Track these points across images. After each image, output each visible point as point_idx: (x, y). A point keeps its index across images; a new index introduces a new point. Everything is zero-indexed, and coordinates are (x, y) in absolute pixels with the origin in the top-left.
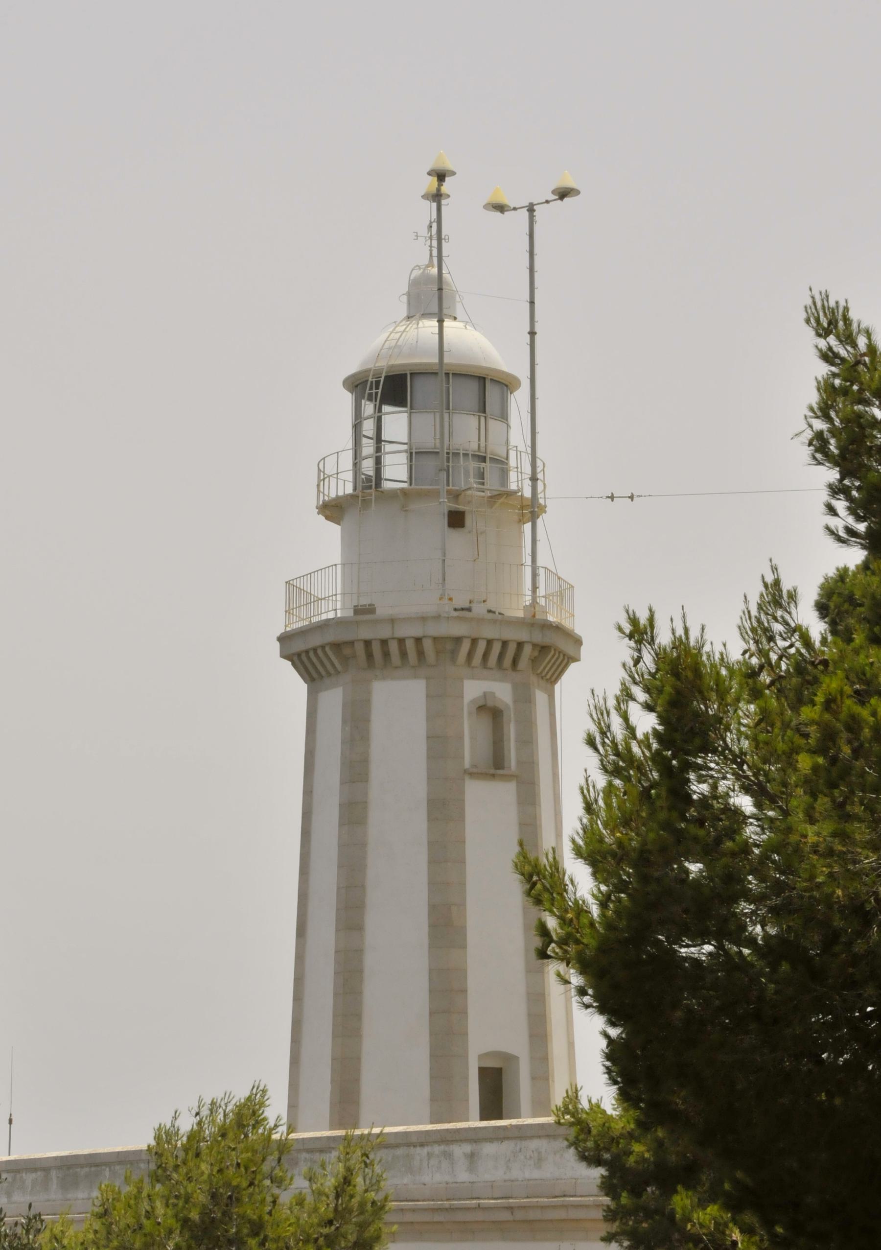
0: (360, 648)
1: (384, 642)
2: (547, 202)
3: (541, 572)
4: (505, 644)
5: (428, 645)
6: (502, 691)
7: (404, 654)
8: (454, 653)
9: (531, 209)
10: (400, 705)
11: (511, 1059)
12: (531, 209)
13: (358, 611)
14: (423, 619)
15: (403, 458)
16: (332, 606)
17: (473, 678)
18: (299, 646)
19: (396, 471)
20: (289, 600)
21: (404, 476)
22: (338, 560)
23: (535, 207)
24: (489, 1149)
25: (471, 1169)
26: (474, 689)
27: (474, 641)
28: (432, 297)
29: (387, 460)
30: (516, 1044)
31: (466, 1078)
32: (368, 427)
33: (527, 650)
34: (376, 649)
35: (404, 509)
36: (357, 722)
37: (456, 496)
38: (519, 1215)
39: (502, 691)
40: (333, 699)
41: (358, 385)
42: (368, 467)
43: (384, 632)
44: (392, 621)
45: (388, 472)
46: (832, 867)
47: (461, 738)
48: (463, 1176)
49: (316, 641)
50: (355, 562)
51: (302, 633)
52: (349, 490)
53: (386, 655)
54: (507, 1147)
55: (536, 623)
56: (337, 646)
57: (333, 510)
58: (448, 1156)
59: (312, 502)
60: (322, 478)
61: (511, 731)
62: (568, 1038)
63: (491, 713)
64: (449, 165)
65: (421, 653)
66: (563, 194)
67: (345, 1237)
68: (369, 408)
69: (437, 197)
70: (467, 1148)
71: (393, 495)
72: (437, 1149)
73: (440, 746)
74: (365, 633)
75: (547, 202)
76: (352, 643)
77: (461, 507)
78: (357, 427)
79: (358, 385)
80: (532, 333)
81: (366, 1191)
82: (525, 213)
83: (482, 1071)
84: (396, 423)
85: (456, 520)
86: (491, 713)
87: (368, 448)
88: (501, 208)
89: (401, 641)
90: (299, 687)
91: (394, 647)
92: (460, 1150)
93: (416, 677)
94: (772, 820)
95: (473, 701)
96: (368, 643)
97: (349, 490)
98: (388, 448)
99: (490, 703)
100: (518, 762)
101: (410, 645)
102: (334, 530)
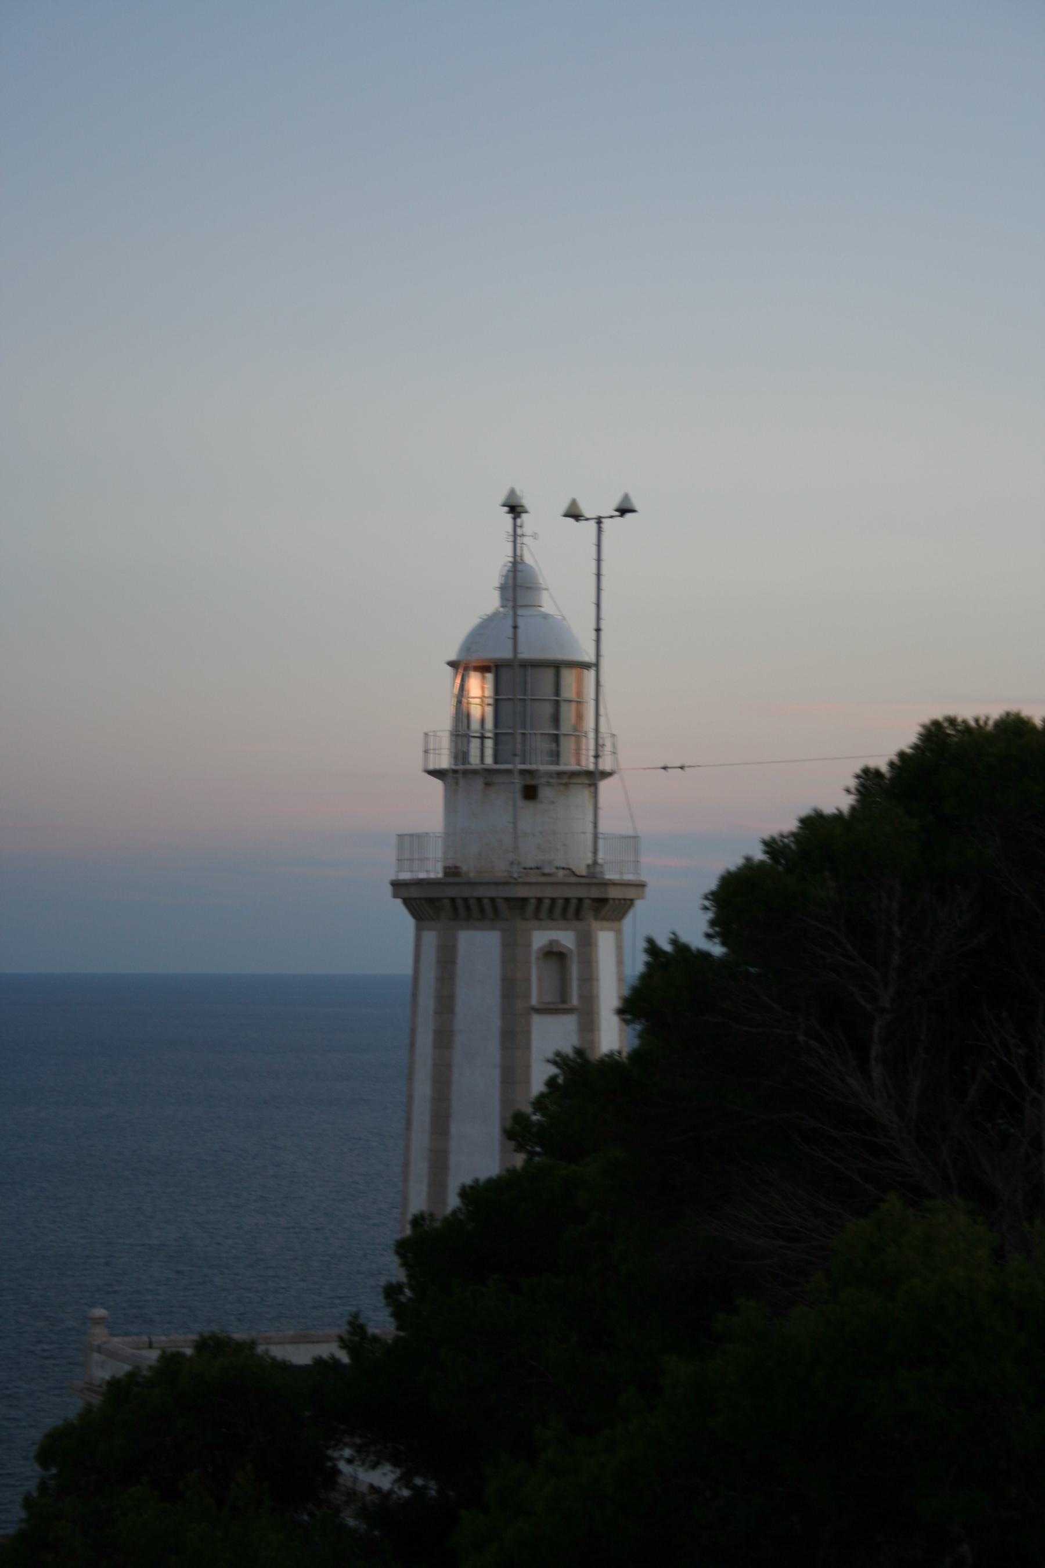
2: (612, 517)
6: (566, 938)
9: (599, 521)
10: (480, 947)
12: (599, 521)
17: (540, 929)
18: (414, 893)
23: (603, 520)
26: (540, 938)
33: (587, 902)
39: (566, 938)
43: (466, 892)
47: (528, 980)
55: (593, 878)
61: (574, 971)
62: (459, 702)
63: (555, 955)
73: (511, 988)
74: (452, 892)
75: (612, 517)
76: (439, 899)
77: (533, 782)
82: (592, 525)
85: (530, 793)
90: (408, 922)
93: (493, 928)
95: (541, 949)
96: (453, 900)
99: (555, 950)
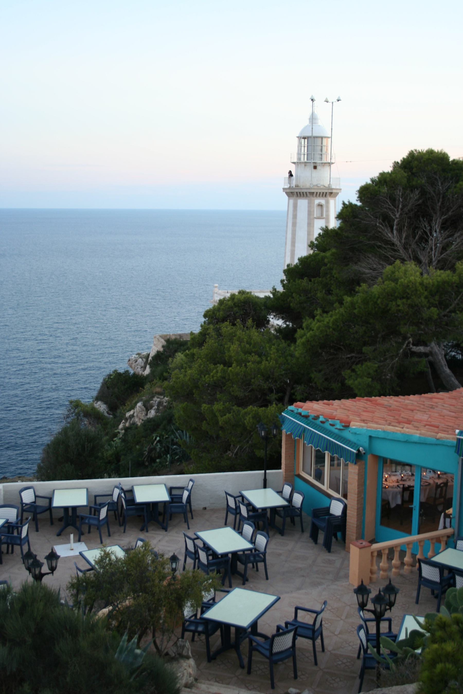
0: (295, 193)
4: (323, 193)
5: (308, 193)
9: (333, 103)
10: (303, 203)
14: (307, 189)
27: (317, 193)
28: (313, 119)
33: (328, 193)
36: (295, 206)
43: (300, 191)
47: (314, 211)
55: (329, 188)
63: (320, 205)
67: (370, 286)
73: (310, 213)
80: (332, 129)
81: (391, 344)
85: (315, 167)
88: (327, 102)
89: (303, 193)
94: (97, 511)
96: (297, 193)
100: (326, 215)
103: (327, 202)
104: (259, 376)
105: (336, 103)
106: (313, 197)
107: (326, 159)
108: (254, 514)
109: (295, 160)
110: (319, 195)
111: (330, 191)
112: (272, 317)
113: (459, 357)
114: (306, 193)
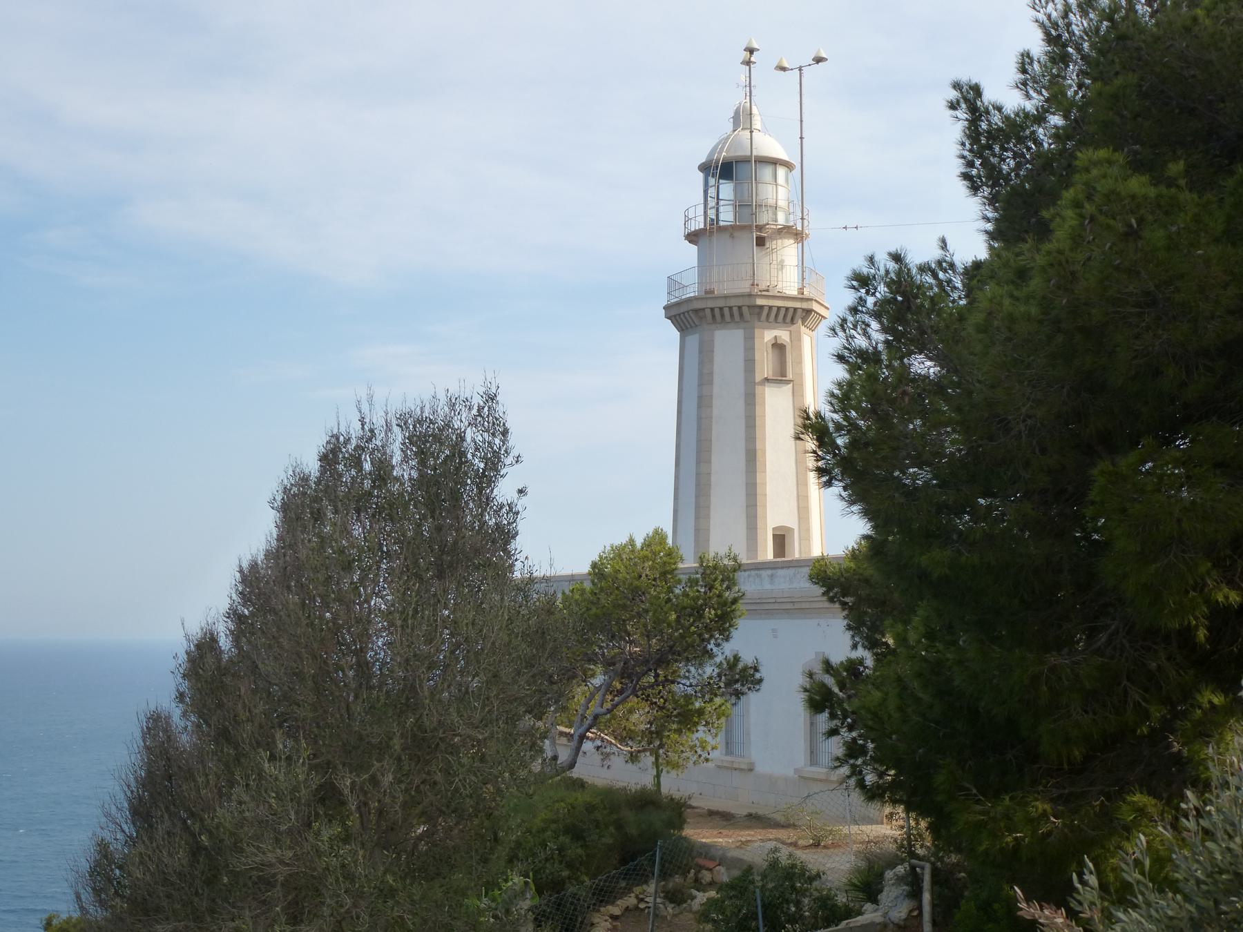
0: (708, 312)
1: (721, 309)
3: (807, 271)
4: (787, 309)
7: (732, 315)
8: (759, 314)
10: (727, 341)
11: (790, 530)
13: (706, 292)
15: (731, 208)
16: (691, 292)
19: (727, 216)
20: (669, 286)
21: (732, 219)
22: (695, 262)
24: (780, 572)
25: (772, 582)
28: (742, 118)
29: (721, 209)
30: (791, 521)
31: (766, 540)
32: (712, 192)
33: (799, 312)
34: (717, 312)
35: (732, 236)
37: (760, 228)
38: (797, 606)
39: (783, 335)
40: (693, 339)
41: (705, 168)
42: (712, 214)
43: (721, 303)
44: (726, 297)
45: (722, 217)
46: (976, 519)
48: (768, 586)
49: (684, 308)
50: (704, 264)
51: (678, 304)
52: (702, 226)
53: (722, 316)
54: (791, 571)
56: (696, 311)
57: (693, 237)
58: (759, 576)
59: (681, 233)
60: (687, 220)
63: (779, 347)
64: (755, 46)
65: (741, 315)
66: (819, 60)
68: (712, 181)
69: (748, 63)
70: (769, 572)
71: (724, 229)
72: (753, 573)
74: (710, 304)
78: (706, 192)
79: (705, 168)
82: (797, 71)
83: (775, 536)
84: (727, 189)
86: (779, 347)
87: (712, 203)
88: (784, 69)
89: (731, 308)
91: (726, 311)
92: (765, 573)
96: (712, 309)
97: (702, 226)
98: (721, 203)
101: (735, 310)
102: (693, 249)
103: (796, 339)
104: (517, 880)
105: (812, 72)
106: (759, 320)
107: (736, 234)
108: (1152, 192)
109: (698, 224)
110: (776, 316)
111: (805, 305)
112: (932, 370)
113: (1234, 597)
114: (740, 308)
